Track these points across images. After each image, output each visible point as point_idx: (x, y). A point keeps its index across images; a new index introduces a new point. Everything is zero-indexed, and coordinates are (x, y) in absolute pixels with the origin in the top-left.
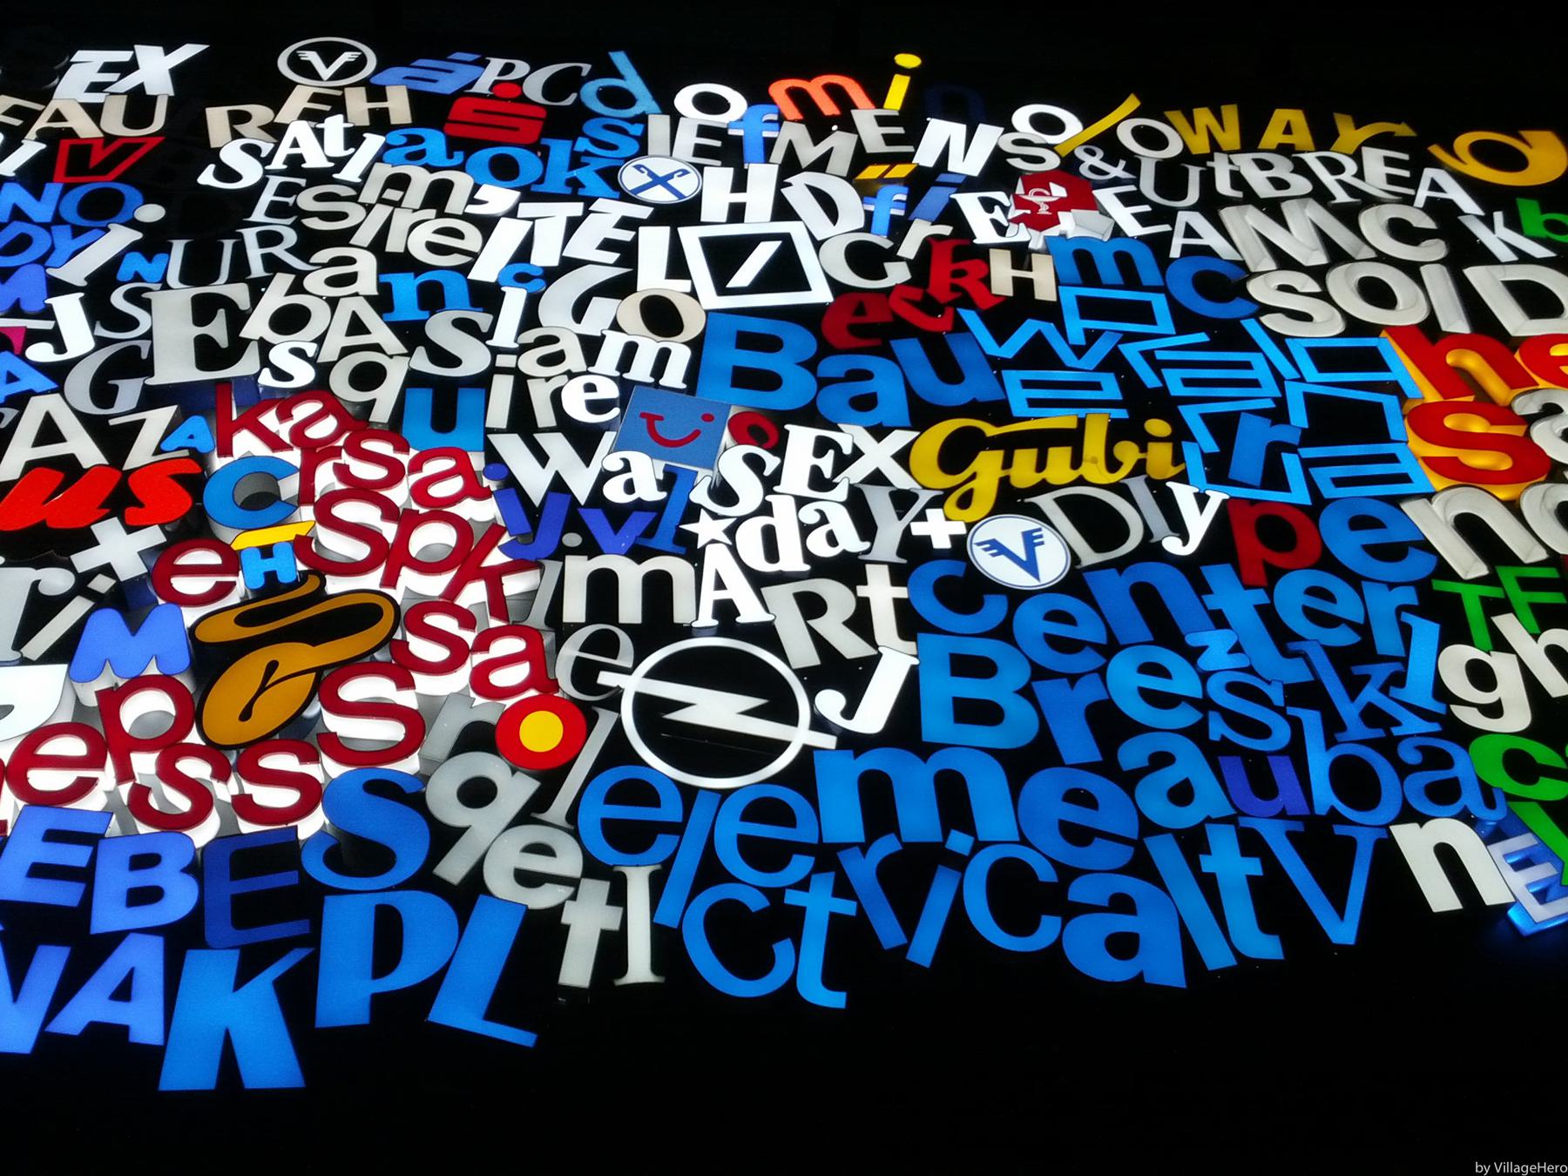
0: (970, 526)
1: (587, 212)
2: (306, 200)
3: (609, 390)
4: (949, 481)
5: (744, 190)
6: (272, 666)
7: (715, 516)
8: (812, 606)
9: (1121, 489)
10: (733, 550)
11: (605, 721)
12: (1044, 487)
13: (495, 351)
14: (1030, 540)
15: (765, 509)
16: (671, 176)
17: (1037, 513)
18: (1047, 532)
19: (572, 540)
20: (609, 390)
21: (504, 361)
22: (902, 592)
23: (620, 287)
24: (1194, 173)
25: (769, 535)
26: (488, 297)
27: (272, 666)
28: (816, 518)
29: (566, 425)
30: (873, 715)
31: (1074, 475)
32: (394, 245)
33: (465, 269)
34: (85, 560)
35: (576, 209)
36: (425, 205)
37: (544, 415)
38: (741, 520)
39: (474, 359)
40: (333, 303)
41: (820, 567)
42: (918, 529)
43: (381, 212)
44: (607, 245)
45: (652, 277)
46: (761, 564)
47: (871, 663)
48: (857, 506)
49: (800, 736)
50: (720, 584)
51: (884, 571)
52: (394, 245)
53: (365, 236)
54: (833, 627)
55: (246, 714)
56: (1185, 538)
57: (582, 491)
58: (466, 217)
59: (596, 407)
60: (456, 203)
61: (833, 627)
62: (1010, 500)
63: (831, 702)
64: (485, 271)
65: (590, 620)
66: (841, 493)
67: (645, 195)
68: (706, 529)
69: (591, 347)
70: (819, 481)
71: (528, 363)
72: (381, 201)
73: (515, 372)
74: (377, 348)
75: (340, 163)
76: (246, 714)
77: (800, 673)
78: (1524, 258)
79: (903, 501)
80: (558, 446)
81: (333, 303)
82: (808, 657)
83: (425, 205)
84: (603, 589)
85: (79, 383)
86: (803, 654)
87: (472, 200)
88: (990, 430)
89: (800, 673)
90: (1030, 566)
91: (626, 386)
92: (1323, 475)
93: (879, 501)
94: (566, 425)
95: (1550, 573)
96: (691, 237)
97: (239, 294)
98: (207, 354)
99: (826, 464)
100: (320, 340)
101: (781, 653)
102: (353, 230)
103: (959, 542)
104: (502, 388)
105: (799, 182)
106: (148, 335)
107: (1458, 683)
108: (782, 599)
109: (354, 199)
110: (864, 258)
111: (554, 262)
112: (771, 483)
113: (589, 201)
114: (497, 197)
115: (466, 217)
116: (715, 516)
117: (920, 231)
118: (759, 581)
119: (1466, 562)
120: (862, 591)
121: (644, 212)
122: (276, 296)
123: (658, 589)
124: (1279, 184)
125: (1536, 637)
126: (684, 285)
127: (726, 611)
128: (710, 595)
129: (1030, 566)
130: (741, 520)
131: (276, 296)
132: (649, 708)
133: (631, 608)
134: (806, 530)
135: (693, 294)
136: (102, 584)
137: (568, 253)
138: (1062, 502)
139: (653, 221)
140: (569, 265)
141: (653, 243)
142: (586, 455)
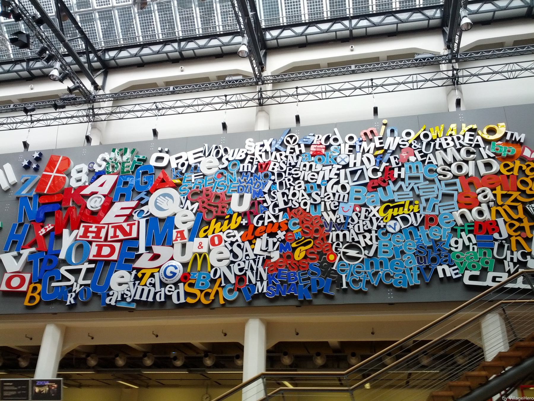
0: (386, 223)
1: (332, 168)
2: (292, 172)
3: (337, 204)
4: (384, 215)
5: (400, 171)
6: (301, 250)
7: (352, 224)
8: (365, 237)
9: (409, 215)
10: (354, 230)
11: (339, 255)
12: (398, 215)
13: (321, 198)
14: (395, 224)
15: (358, 223)
16: (344, 159)
17: (396, 220)
18: (398, 223)
19: (333, 229)
20: (337, 204)
21: (323, 200)
22: (376, 234)
23: (337, 183)
24: (433, 143)
25: (359, 226)
26: (319, 186)
27: (301, 250)
28: (365, 223)
29: (332, 210)
30: (371, 254)
31: (403, 212)
32: (306, 179)
33: (316, 182)
34: (278, 237)
35: (330, 167)
36: (309, 170)
37: (329, 209)
38: (355, 224)
39: (319, 200)
40: (299, 191)
41: (365, 231)
42: (379, 224)
43: (303, 172)
44: (336, 174)
45: (343, 181)
46: (358, 232)
47: (372, 245)
48: (371, 221)
49: (362, 256)
50: (352, 235)
51: (374, 231)
52: (306, 179)
53: (301, 178)
54: (367, 240)
55: (299, 256)
56: (417, 223)
57: (334, 221)
58: (314, 172)
59: (335, 207)
60: (313, 170)
61: (367, 240)
62: (393, 218)
63: (366, 252)
64: (319, 182)
65: (336, 241)
66: (369, 219)
67: (340, 163)
68: (350, 226)
69: (334, 194)
70: (366, 217)
71: (326, 199)
72: (303, 170)
73: (324, 201)
74: (306, 199)
75: (296, 163)
76: (299, 256)
77: (363, 247)
78: (489, 157)
79: (377, 219)
80: (330, 213)
81: (299, 191)
82: (364, 245)
83: (309, 170)
84: (338, 236)
85: (271, 208)
86: (363, 245)
87: (316, 168)
88: (391, 205)
89: (363, 247)
90: (394, 229)
91: (339, 202)
92: (441, 209)
93: (374, 219)
94: (332, 210)
95: (473, 224)
96: (348, 170)
97: (287, 191)
98: (286, 203)
99: (367, 214)
100: (298, 199)
101: (360, 245)
102: (299, 177)
103: (385, 226)
104: (323, 203)
105: (365, 156)
106: (277, 200)
107: (453, 244)
108: (361, 237)
109: (299, 170)
110: (375, 171)
111: (328, 179)
112: (359, 218)
113: (332, 165)
114: (319, 167)
115: (314, 172)
116: (352, 224)
117: (384, 164)
118: (357, 234)
119: (460, 221)
120: (371, 234)
121: (341, 167)
122: (292, 191)
123: (345, 235)
124: (448, 144)
125: (467, 235)
126: (347, 181)
127: (353, 239)
128: (351, 237)
129: (394, 229)
130: (355, 224)
131: (292, 191)
132: (344, 253)
133: (341, 239)
134: (364, 225)
135: (348, 183)
136: (280, 240)
137: (330, 177)
138: (401, 218)
139: (342, 168)
140: (330, 179)
141: (342, 172)
142: (334, 214)
